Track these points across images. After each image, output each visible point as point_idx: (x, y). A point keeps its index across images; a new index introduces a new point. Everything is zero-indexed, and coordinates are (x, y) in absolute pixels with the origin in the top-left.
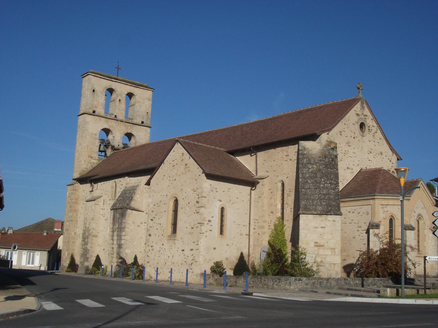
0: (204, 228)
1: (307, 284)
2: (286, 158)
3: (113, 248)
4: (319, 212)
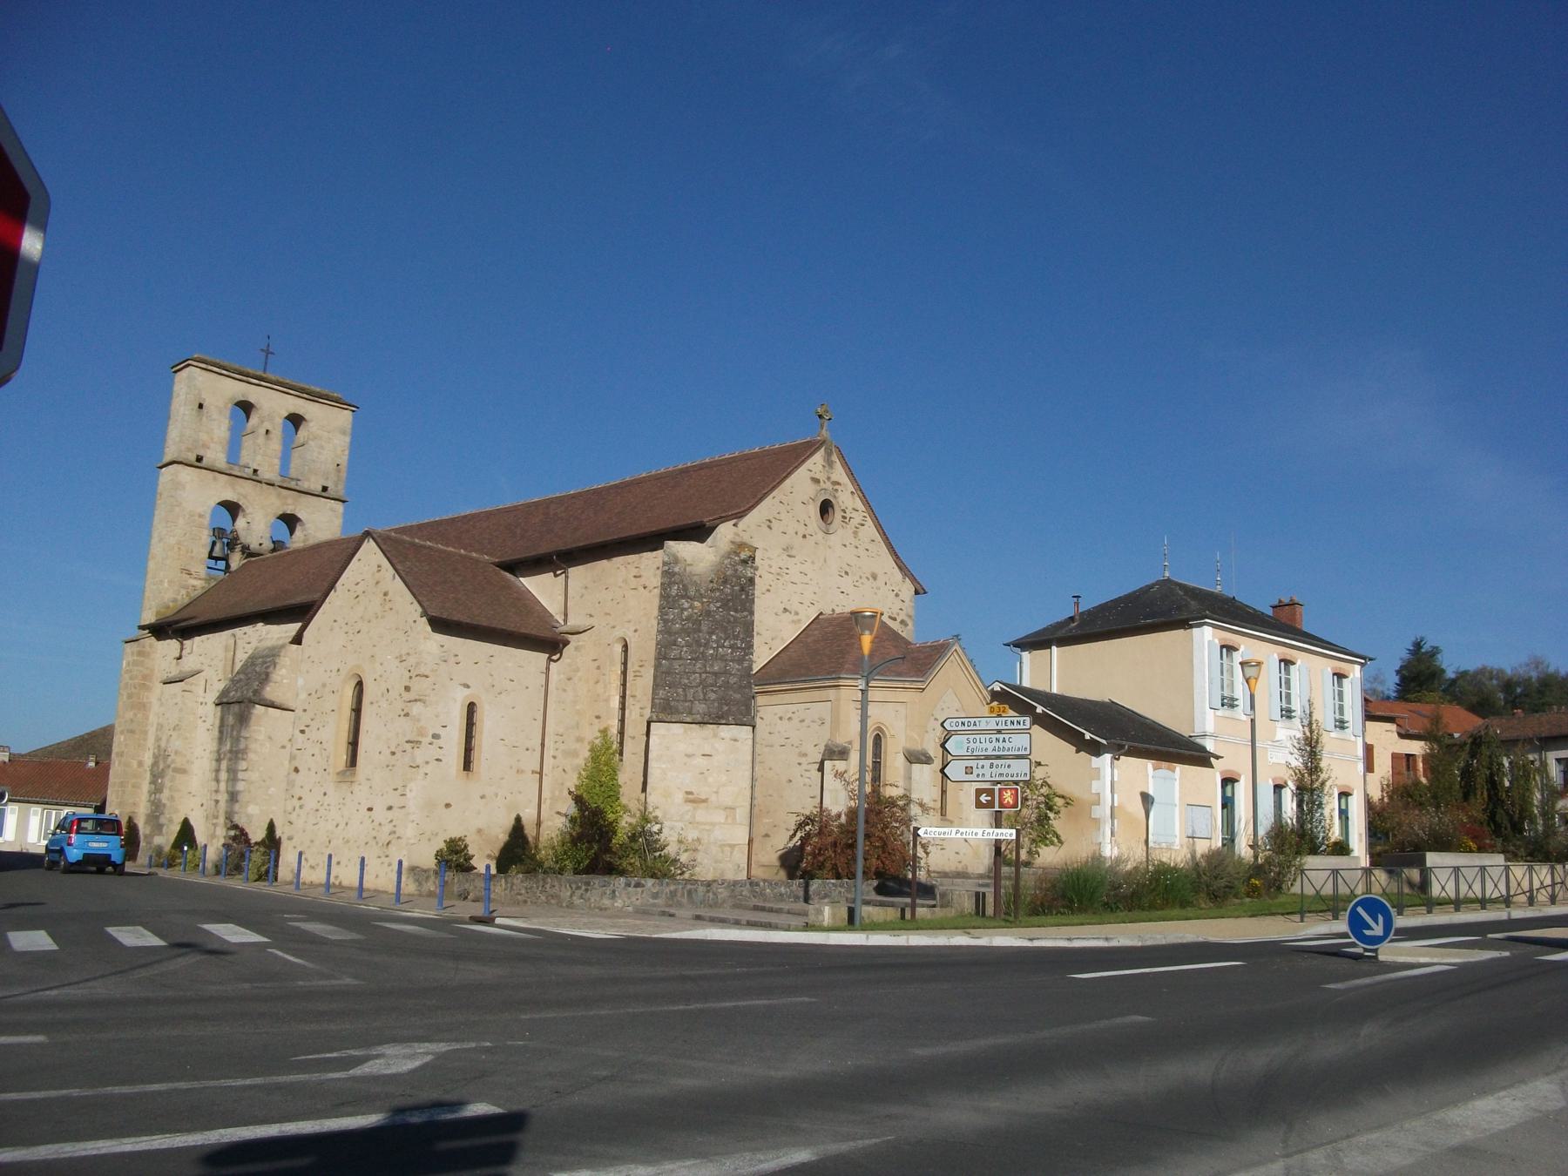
0: (420, 755)
1: (655, 896)
2: (634, 583)
3: (217, 802)
4: (698, 718)
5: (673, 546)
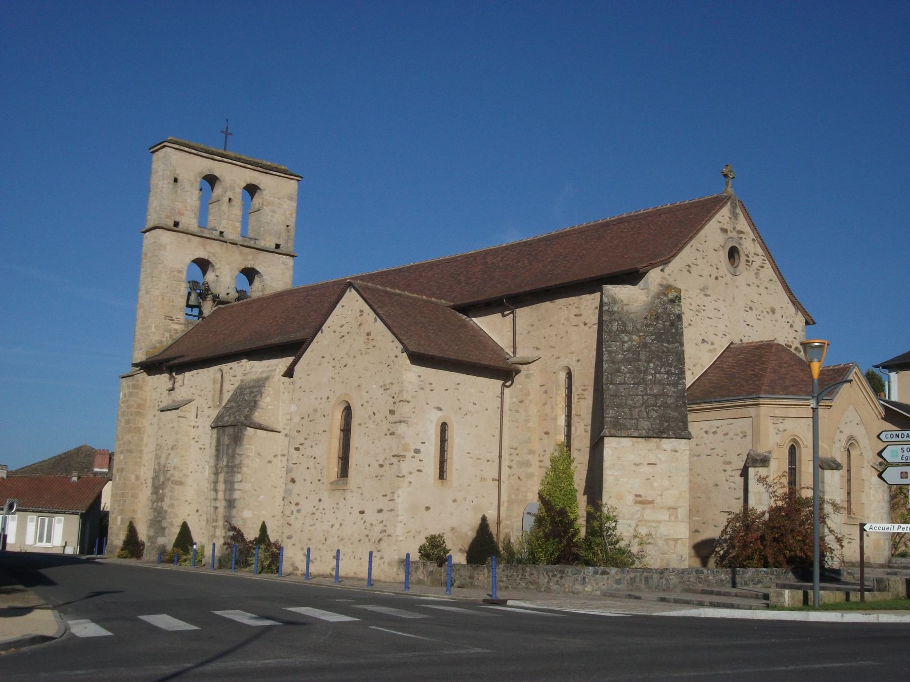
0: (405, 467)
1: (618, 582)
2: (575, 320)
3: (216, 508)
4: (644, 433)
5: (612, 290)
